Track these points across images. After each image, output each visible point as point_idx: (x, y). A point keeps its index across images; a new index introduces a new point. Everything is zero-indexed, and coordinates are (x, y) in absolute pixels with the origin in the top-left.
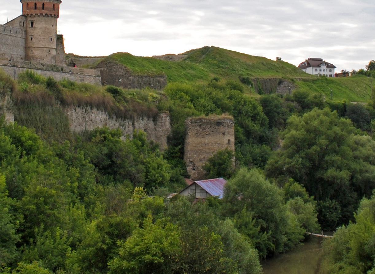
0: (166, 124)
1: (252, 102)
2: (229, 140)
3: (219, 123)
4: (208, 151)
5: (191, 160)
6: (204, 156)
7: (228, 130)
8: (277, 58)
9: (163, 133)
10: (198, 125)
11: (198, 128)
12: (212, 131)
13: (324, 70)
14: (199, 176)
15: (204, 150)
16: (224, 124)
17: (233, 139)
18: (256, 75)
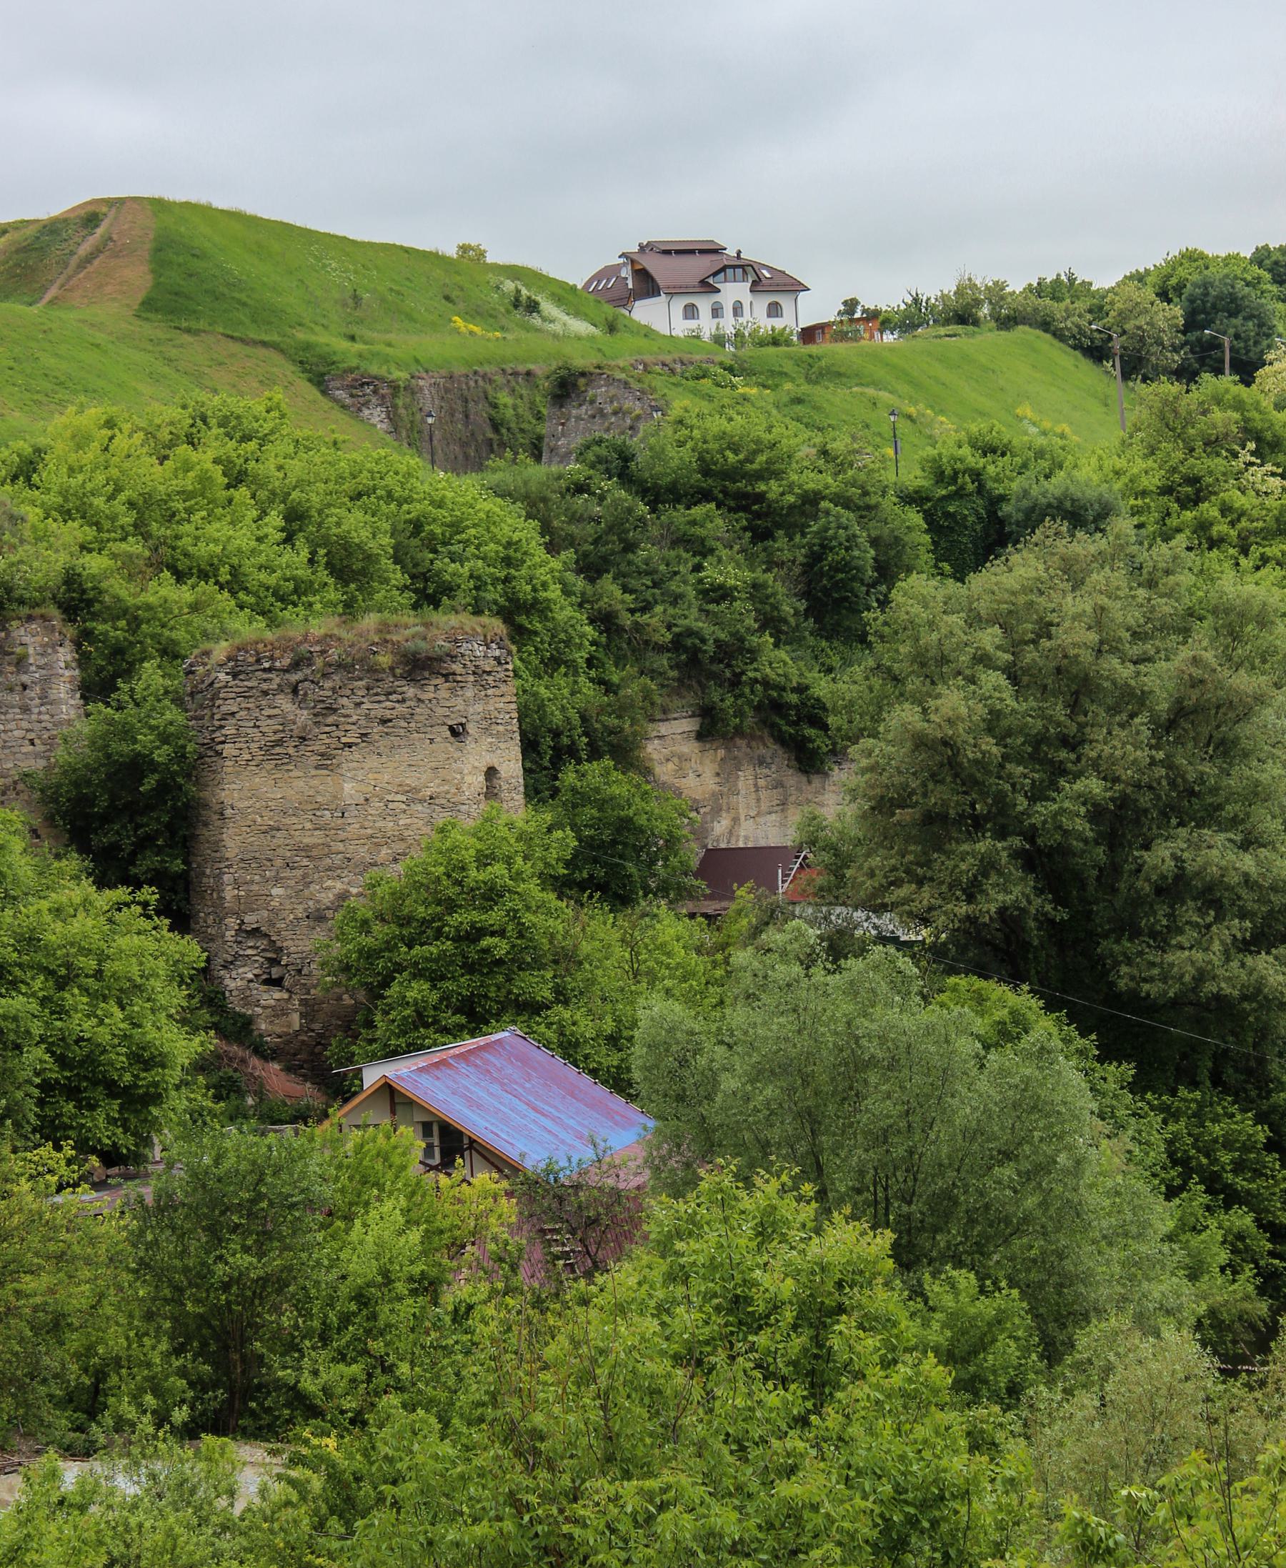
0: (53, 694)
1: (990, 484)
2: (491, 772)
3: (419, 666)
4: (362, 853)
5: (251, 920)
6: (339, 886)
7: (479, 708)
8: (464, 249)
9: (37, 756)
10: (280, 689)
11: (285, 704)
12: (384, 721)
13: (738, 309)
14: (317, 1026)
15: (341, 847)
16: (457, 667)
17: (511, 766)
18: (405, 349)
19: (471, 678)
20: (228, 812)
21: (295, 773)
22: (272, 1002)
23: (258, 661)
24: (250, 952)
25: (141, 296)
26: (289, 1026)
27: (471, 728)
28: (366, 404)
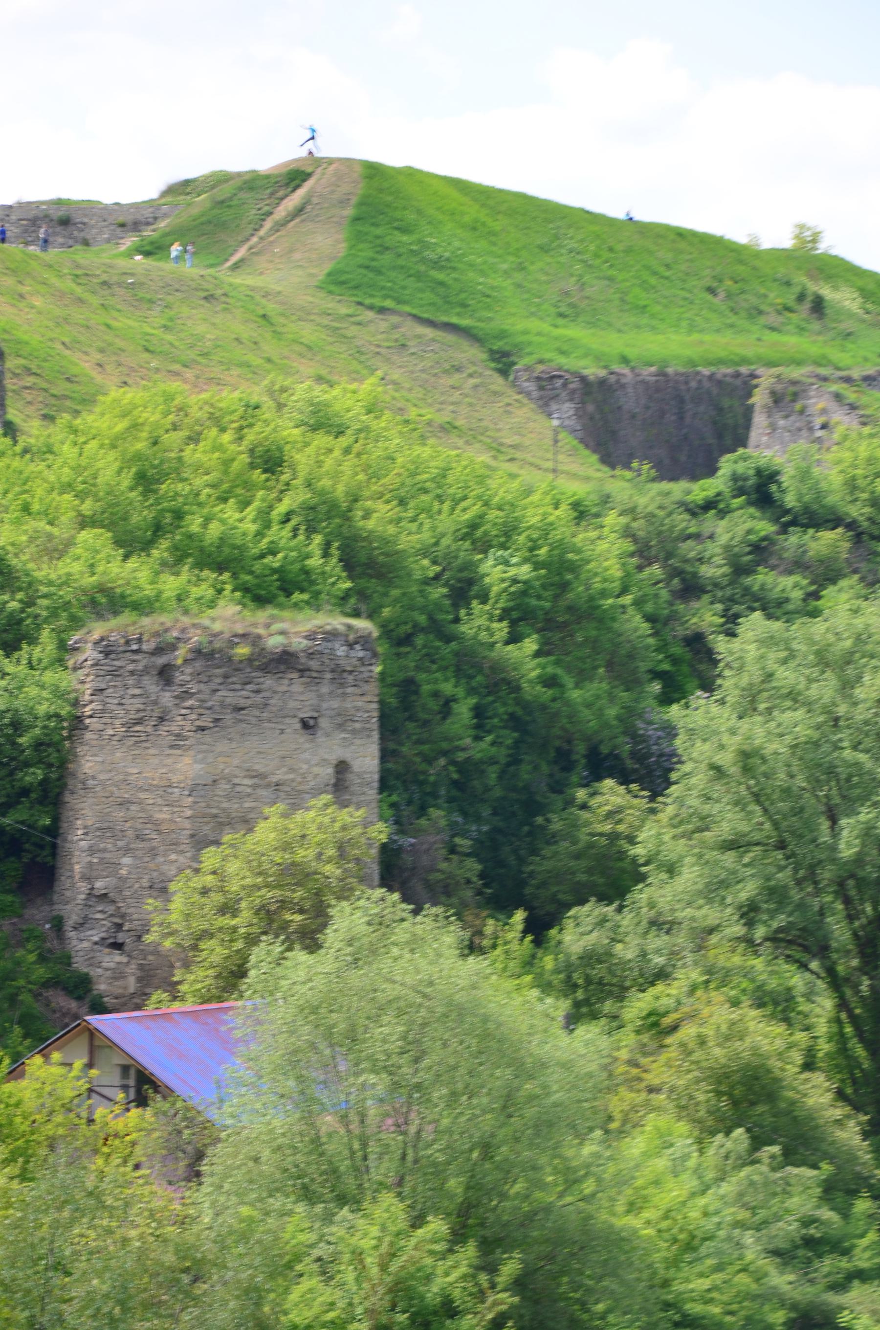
2: (342, 767)
7: (335, 704)
19: (328, 676)
20: (91, 782)
21: (152, 751)
22: (112, 965)
23: (128, 642)
24: (99, 916)
25: (328, 267)
26: (125, 988)
27: (324, 723)
28: (555, 397)
